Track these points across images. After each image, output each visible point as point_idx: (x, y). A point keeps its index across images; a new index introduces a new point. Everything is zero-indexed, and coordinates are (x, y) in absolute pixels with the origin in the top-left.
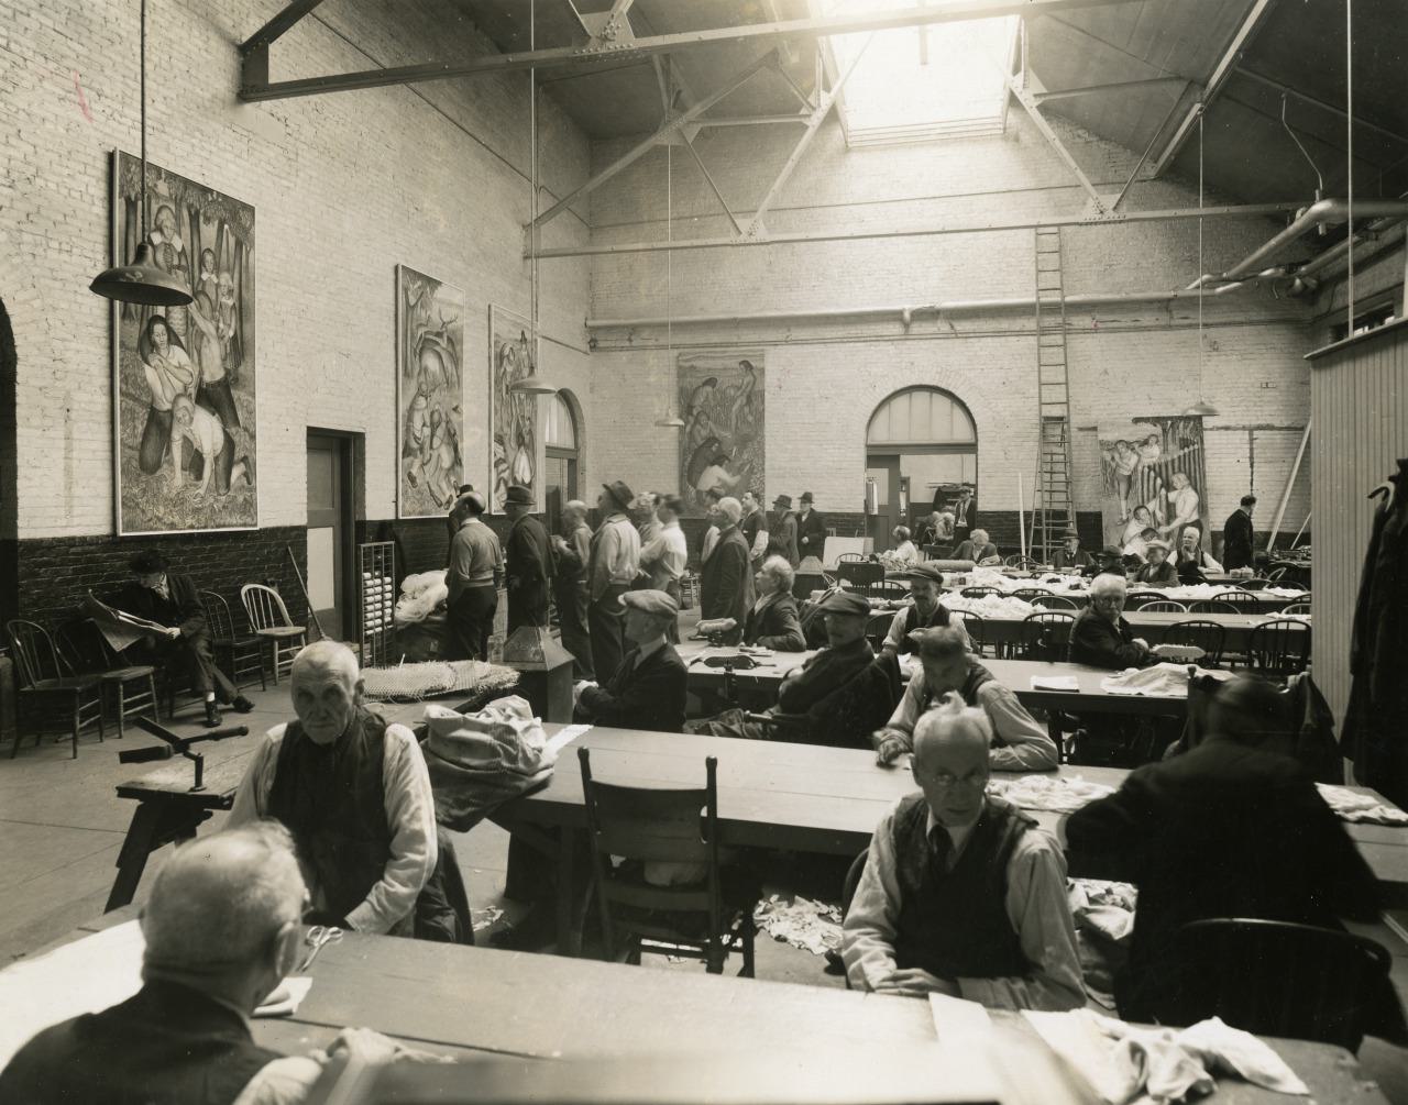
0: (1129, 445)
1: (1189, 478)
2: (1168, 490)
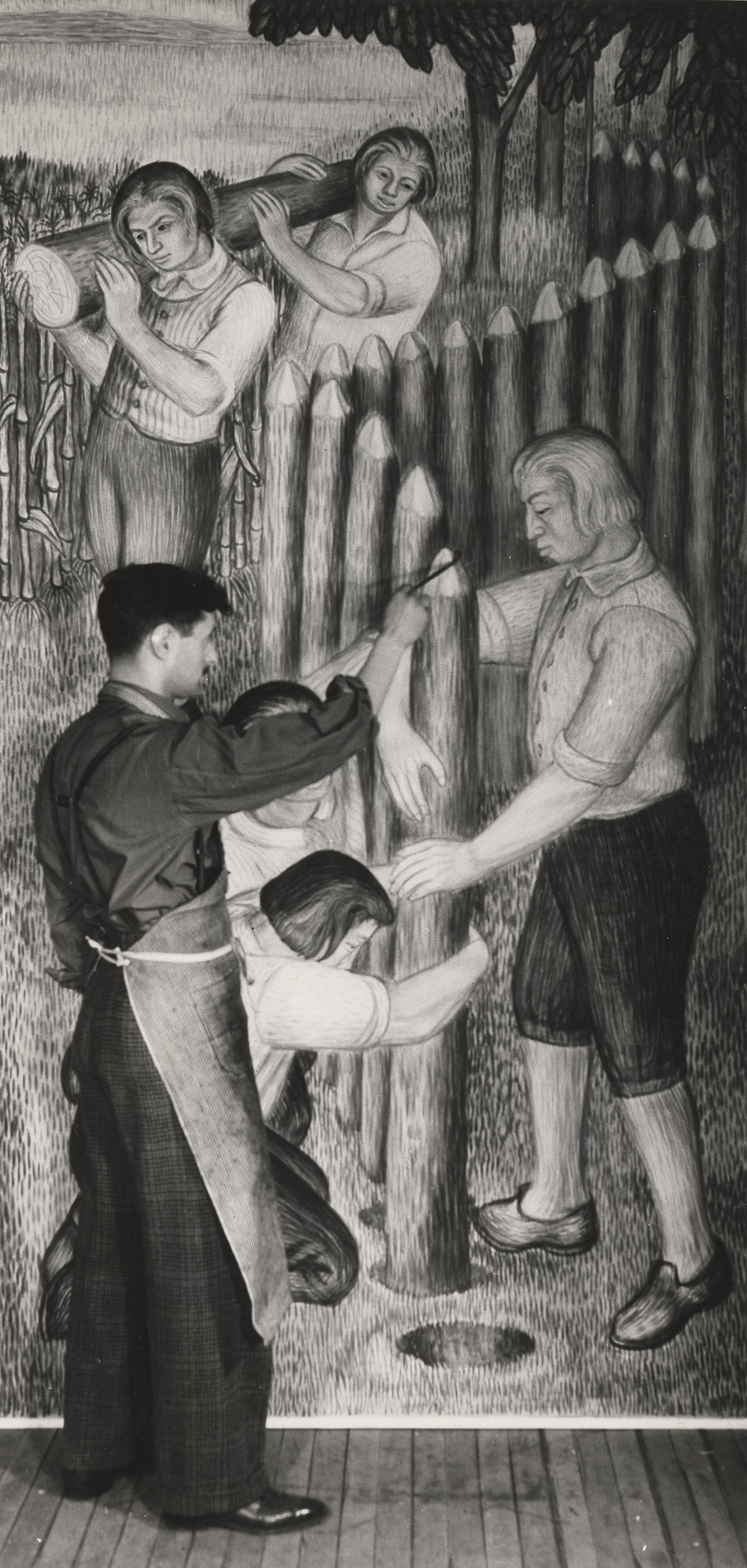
0: (208, 201)
1: (636, 479)
2: (480, 571)
